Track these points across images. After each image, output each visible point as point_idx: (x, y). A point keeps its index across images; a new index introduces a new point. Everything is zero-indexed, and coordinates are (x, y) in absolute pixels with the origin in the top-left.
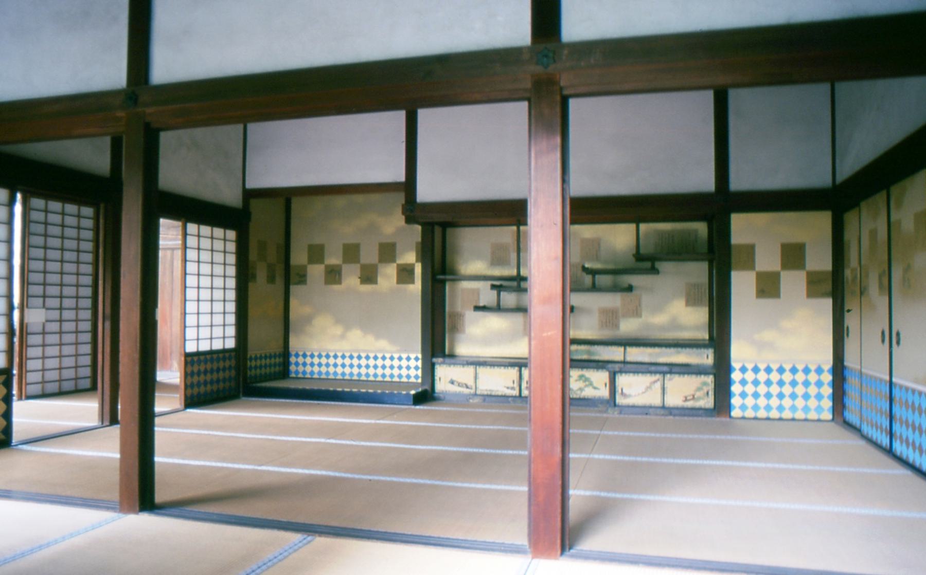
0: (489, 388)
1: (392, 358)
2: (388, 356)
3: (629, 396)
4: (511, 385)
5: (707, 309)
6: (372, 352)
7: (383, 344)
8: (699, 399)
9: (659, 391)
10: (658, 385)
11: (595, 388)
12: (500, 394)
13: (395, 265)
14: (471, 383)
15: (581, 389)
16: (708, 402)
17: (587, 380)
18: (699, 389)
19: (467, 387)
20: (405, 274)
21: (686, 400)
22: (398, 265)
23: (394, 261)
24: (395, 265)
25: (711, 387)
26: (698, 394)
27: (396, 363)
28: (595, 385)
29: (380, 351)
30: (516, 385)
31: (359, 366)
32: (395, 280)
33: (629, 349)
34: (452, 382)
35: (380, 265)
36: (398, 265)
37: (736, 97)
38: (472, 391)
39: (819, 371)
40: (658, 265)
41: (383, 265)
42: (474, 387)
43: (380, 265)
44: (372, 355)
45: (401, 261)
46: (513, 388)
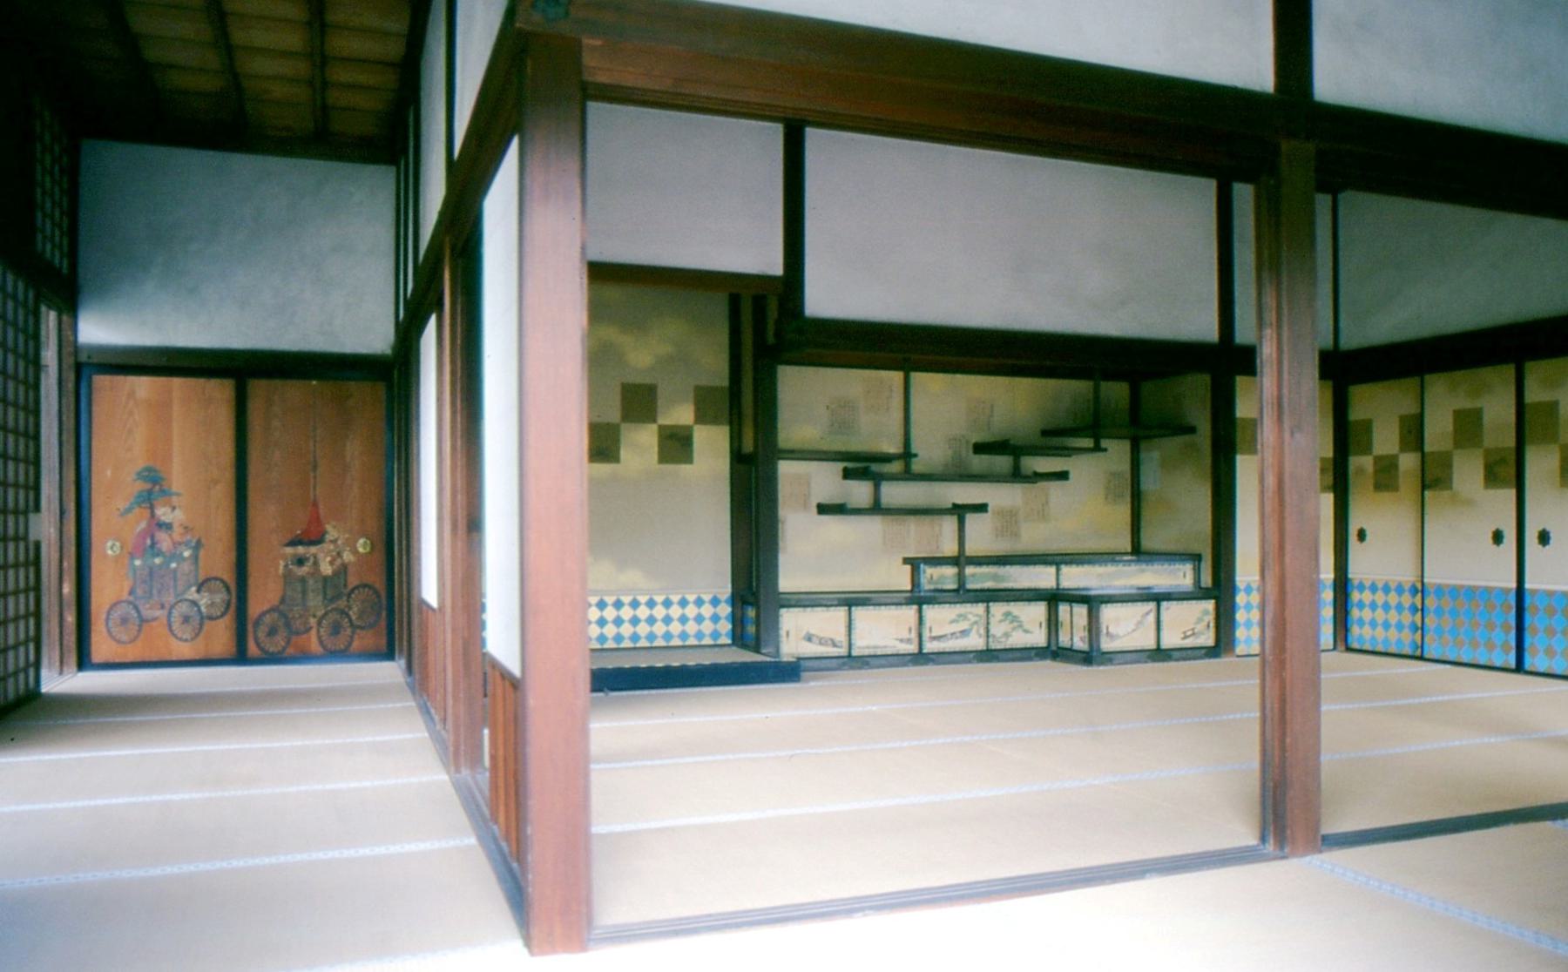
0: (872, 643)
1: (651, 604)
2: (643, 599)
3: (1118, 637)
4: (906, 635)
5: (1128, 507)
6: (610, 593)
7: (632, 576)
8: (1201, 633)
9: (1153, 626)
10: (1152, 618)
11: (1026, 631)
12: (889, 652)
13: (654, 427)
14: (841, 637)
15: (1007, 635)
16: (1208, 639)
17: (1015, 619)
18: (1200, 620)
19: (834, 645)
20: (676, 445)
21: (1186, 637)
22: (661, 428)
23: (654, 421)
24: (654, 427)
25: (1211, 618)
26: (1199, 627)
27: (675, 611)
28: (1027, 627)
29: (627, 592)
30: (914, 635)
31: (683, 620)
32: (656, 457)
33: (1065, 569)
34: (809, 638)
35: (624, 426)
36: (661, 428)
37: (816, 140)
38: (843, 651)
39: (715, 602)
40: (1104, 443)
41: (633, 426)
42: (845, 644)
43: (624, 426)
44: (610, 600)
45: (665, 420)
46: (909, 641)
